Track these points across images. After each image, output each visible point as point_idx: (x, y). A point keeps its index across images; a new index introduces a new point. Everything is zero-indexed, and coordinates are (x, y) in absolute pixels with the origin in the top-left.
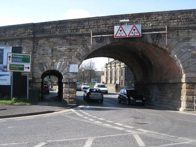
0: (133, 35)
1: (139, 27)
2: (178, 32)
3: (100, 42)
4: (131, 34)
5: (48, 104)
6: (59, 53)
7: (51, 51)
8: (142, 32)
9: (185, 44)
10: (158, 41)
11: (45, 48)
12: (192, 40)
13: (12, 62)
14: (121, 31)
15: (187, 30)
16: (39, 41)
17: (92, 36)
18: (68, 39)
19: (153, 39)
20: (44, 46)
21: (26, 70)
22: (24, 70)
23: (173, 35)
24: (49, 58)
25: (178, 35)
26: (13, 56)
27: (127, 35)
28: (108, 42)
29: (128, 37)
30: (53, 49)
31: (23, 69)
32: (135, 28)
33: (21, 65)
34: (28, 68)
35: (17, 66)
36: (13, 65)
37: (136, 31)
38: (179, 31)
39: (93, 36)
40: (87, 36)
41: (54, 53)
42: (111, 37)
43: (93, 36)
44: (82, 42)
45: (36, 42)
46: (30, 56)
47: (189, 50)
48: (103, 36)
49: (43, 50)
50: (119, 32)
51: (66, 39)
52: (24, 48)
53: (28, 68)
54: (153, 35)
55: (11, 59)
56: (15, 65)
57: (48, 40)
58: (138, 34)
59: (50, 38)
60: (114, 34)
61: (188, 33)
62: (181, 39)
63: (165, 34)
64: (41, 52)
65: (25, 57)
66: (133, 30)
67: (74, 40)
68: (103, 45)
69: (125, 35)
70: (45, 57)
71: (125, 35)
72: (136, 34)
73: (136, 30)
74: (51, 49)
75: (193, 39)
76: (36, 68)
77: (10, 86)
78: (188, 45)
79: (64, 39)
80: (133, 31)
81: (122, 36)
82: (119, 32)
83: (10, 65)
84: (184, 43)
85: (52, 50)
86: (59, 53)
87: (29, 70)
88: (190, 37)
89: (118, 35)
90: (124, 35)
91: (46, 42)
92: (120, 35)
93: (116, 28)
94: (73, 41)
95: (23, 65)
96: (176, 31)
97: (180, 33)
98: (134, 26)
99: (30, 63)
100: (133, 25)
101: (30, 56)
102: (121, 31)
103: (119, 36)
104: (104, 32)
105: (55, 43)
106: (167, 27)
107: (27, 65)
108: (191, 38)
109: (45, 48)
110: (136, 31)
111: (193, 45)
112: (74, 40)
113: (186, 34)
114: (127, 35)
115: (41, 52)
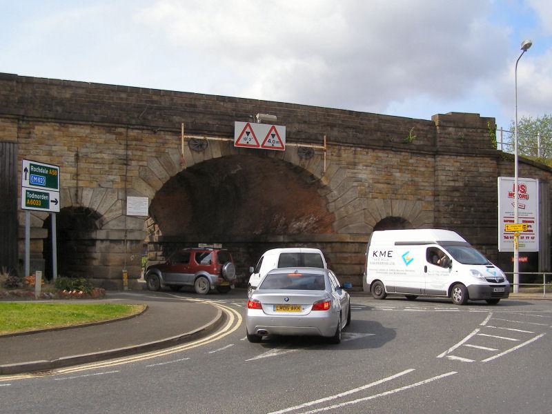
0: (270, 145)
2: (339, 150)
3: (198, 152)
4: (267, 144)
6: (96, 167)
7: (72, 159)
9: (348, 173)
10: (308, 162)
11: (54, 148)
12: (359, 167)
13: (30, 184)
14: (248, 133)
15: (353, 149)
16: (36, 127)
17: (183, 137)
18: (121, 134)
19: (301, 158)
20: (50, 142)
22: (48, 207)
23: (332, 155)
24: (68, 176)
25: (339, 156)
27: (261, 144)
28: (217, 154)
29: (260, 148)
30: (80, 155)
32: (275, 133)
38: (342, 148)
39: (232, 140)
40: (170, 133)
41: (82, 165)
42: (492, 189)
44: (156, 146)
45: (25, 128)
47: (355, 184)
49: (50, 153)
50: (245, 134)
51: (114, 133)
54: (300, 149)
57: (62, 128)
58: (280, 146)
59: (71, 126)
60: (233, 136)
61: (355, 154)
63: (322, 150)
67: (136, 139)
68: (206, 159)
69: (256, 144)
71: (256, 144)
72: (276, 145)
73: (276, 136)
74: (73, 154)
75: (361, 165)
78: (353, 175)
79: (109, 132)
80: (270, 137)
81: (251, 146)
82: (245, 134)
83: (27, 191)
84: (348, 170)
86: (96, 167)
88: (357, 161)
90: (253, 142)
92: (245, 143)
93: (239, 126)
94: (132, 140)
95: (47, 194)
96: (337, 147)
98: (248, 125)
100: (245, 123)
102: (248, 133)
103: (245, 145)
105: (83, 140)
106: (327, 137)
108: (359, 163)
109: (54, 148)
111: (360, 176)
112: (136, 139)
113: (351, 155)
114: (261, 144)
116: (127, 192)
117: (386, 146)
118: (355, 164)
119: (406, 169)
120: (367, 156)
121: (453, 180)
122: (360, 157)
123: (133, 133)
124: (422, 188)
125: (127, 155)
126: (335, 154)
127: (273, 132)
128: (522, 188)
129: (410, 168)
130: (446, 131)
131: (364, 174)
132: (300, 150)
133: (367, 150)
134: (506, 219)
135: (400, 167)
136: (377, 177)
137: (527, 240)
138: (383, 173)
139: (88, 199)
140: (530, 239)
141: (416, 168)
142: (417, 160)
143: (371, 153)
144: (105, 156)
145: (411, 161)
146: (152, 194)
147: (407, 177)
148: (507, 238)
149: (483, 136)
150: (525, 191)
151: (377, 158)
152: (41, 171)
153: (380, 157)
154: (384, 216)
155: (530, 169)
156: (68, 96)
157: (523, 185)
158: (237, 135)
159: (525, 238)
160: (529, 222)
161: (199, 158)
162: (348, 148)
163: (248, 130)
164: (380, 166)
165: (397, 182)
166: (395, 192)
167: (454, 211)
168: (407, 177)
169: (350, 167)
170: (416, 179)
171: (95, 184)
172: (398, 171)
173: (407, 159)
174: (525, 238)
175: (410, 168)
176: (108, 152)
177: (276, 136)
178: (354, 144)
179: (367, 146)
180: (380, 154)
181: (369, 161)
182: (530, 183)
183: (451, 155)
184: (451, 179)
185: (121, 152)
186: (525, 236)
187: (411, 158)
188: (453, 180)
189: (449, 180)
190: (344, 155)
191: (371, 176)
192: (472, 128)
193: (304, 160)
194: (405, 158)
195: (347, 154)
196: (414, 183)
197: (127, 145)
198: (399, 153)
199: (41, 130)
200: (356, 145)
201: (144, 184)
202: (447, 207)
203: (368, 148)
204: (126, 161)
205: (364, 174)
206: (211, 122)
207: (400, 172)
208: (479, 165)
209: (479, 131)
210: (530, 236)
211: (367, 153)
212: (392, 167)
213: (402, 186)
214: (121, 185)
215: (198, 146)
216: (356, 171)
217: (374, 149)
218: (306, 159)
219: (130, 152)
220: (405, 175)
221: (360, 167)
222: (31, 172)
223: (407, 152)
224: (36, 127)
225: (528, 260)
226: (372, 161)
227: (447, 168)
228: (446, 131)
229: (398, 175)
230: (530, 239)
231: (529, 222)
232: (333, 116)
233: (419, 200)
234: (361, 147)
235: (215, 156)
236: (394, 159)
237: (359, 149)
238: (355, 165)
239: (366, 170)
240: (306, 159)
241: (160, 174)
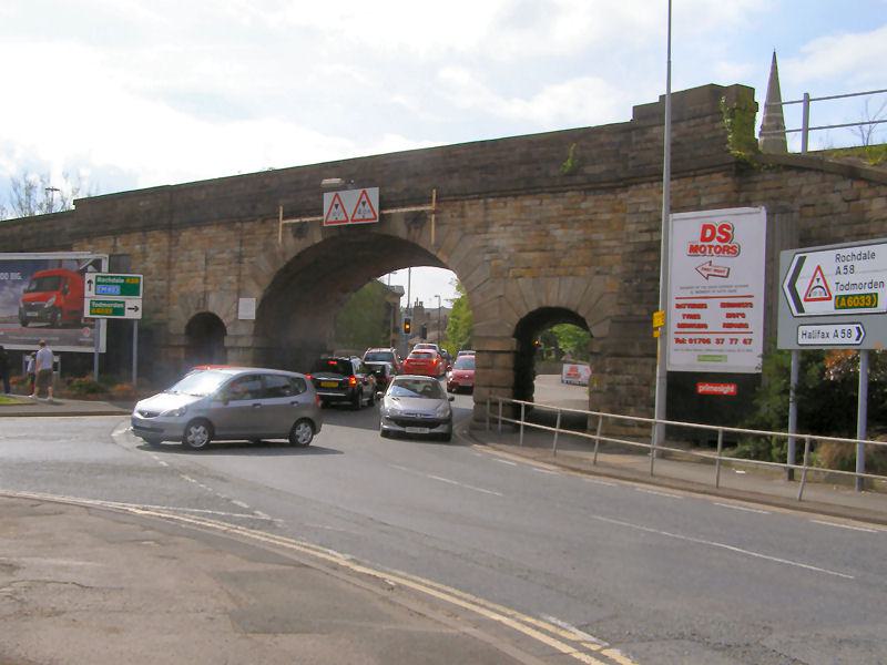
1: (374, 194)
2: (463, 207)
4: (357, 216)
5: (268, 378)
8: (381, 208)
11: (193, 253)
15: (482, 201)
18: (238, 229)
19: (409, 230)
20: (190, 248)
21: (129, 315)
23: (452, 216)
25: (462, 215)
26: (99, 280)
27: (350, 216)
29: (350, 223)
31: (121, 311)
33: (119, 302)
34: (136, 309)
35: (109, 305)
36: (98, 302)
37: (367, 207)
38: (467, 202)
39: (319, 218)
43: (287, 221)
46: (139, 278)
47: (487, 257)
48: (304, 220)
52: (151, 254)
53: (136, 309)
55: (93, 286)
56: (104, 302)
58: (372, 216)
61: (486, 209)
62: (470, 226)
64: (186, 265)
65: (128, 281)
66: (361, 205)
70: (192, 277)
73: (367, 204)
76: (175, 307)
77: (674, 209)
78: (485, 244)
84: (477, 236)
85: (206, 260)
87: (138, 315)
88: (490, 219)
89: (332, 218)
91: (195, 237)
92: (334, 219)
95: (124, 303)
96: (458, 203)
97: (467, 208)
99: (138, 295)
101: (139, 278)
104: (308, 211)
107: (136, 301)
108: (493, 222)
110: (367, 207)
111: (496, 243)
114: (350, 216)
115: (186, 265)
116: (240, 293)
117: (530, 188)
118: (486, 226)
119: (574, 221)
120: (506, 210)
121: (647, 231)
122: (495, 211)
123: (247, 226)
124: (605, 251)
125: (793, 212)
126: (455, 214)
127: (364, 199)
128: (726, 232)
129: (581, 217)
130: (647, 136)
131: (502, 239)
132: (407, 217)
133: (503, 199)
134: (681, 302)
135: (563, 219)
136: (521, 242)
137: (733, 346)
138: (533, 233)
139: (215, 305)
140: (740, 345)
141: (593, 217)
142: (596, 201)
143: (512, 203)
144: (225, 255)
145: (583, 205)
146: (259, 293)
147: (576, 234)
148: (683, 341)
149: (714, 129)
150: (728, 238)
151: (523, 209)
152: (114, 280)
153: (526, 206)
154: (534, 307)
155: (824, 181)
156: (203, 197)
157: (726, 226)
158: (326, 211)
159: (727, 341)
160: (739, 305)
161: (303, 244)
162: (474, 202)
163: (337, 202)
164: (528, 223)
165: (557, 246)
166: (555, 264)
167: (638, 291)
168: (576, 234)
169: (479, 230)
170: (594, 236)
171: (218, 288)
172: (559, 225)
173: (576, 202)
174: (727, 341)
175: (581, 217)
176: (228, 251)
177: (367, 204)
178: (479, 193)
179: (502, 194)
180: (528, 202)
181: (509, 217)
182: (742, 218)
183: (652, 182)
184: (645, 228)
185: (237, 249)
186: (727, 337)
187: (584, 200)
188: (647, 231)
189: (641, 232)
190: (470, 213)
191: (512, 241)
192: (694, 118)
193: (413, 230)
194: (573, 200)
195: (474, 212)
196: (589, 244)
197: (241, 241)
198: (560, 194)
199: (186, 235)
200: (484, 194)
201: (253, 283)
202: (627, 284)
203: (506, 196)
204: (240, 258)
205: (502, 239)
206: (311, 199)
207: (562, 228)
208: (700, 191)
209: (708, 119)
210: (741, 337)
211: (505, 203)
212: (549, 220)
213: (565, 253)
214: (235, 287)
215: (300, 231)
216: (488, 236)
217: (516, 196)
218: (416, 228)
219: (243, 249)
220: (571, 231)
221: (494, 229)
222: (97, 283)
223: (573, 190)
224: (184, 234)
225: (738, 389)
226: (515, 216)
227: (643, 208)
228: (647, 136)
229: (559, 233)
230: (740, 345)
231: (739, 305)
232: (456, 156)
233: (598, 273)
234: (493, 197)
235: (317, 242)
236: (552, 206)
237: (491, 200)
238: (487, 227)
239: (505, 231)
240: (416, 228)
241: (267, 269)
